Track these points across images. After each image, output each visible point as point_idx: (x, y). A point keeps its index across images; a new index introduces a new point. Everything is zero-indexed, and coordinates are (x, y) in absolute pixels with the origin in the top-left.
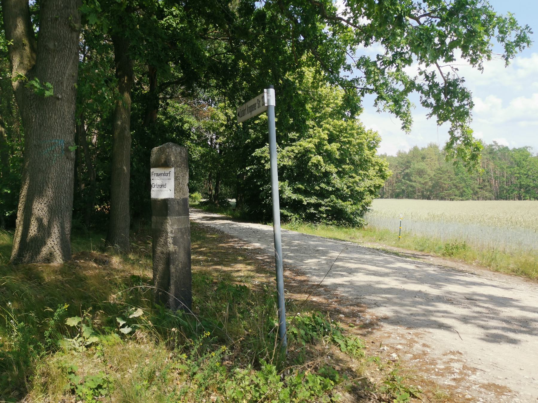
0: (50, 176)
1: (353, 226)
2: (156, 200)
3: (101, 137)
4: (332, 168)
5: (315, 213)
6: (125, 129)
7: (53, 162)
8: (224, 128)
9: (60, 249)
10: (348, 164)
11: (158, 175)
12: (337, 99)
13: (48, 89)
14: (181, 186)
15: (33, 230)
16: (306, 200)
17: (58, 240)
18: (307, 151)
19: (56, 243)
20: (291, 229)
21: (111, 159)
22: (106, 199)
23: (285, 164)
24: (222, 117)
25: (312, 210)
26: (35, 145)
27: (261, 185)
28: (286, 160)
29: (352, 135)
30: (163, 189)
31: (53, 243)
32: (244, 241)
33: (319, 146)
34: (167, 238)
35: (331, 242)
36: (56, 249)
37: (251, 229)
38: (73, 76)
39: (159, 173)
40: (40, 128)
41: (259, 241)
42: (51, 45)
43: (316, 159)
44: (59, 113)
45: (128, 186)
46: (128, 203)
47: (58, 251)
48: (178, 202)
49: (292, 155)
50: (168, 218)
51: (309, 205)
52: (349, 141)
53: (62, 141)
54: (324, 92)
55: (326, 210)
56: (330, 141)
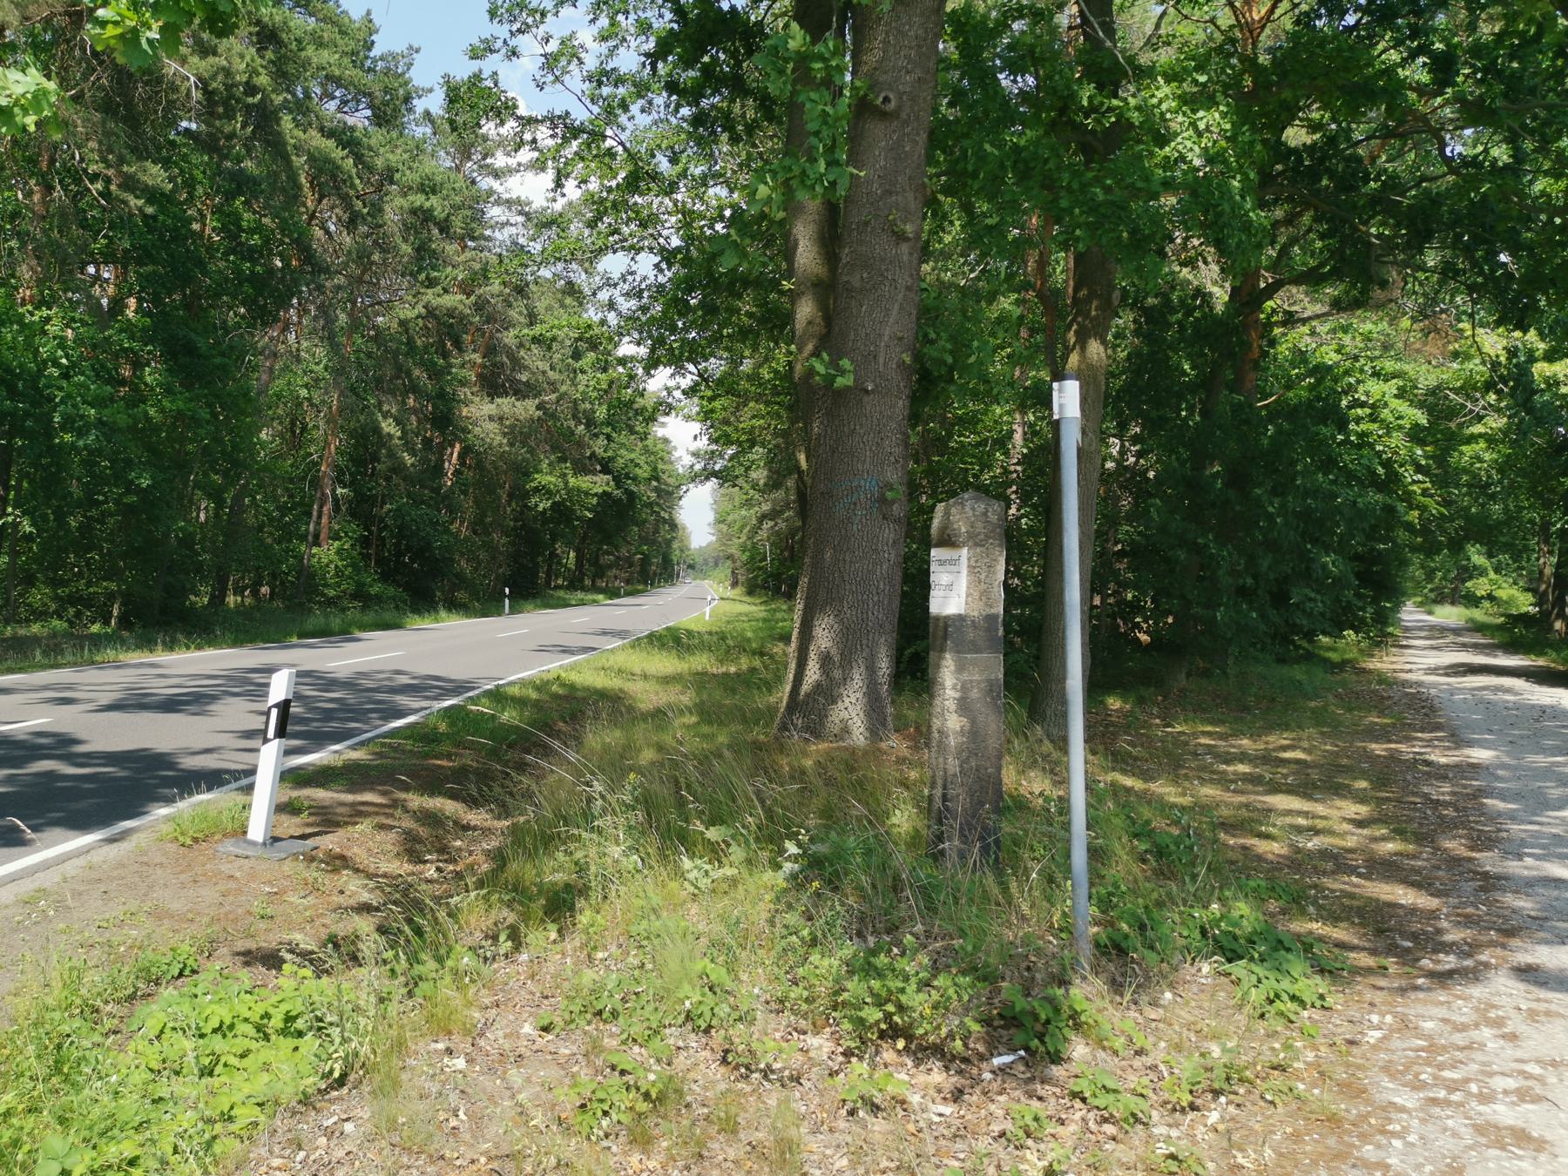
2: (937, 618)
11: (942, 563)
13: (843, 373)
15: (813, 674)
42: (856, 281)
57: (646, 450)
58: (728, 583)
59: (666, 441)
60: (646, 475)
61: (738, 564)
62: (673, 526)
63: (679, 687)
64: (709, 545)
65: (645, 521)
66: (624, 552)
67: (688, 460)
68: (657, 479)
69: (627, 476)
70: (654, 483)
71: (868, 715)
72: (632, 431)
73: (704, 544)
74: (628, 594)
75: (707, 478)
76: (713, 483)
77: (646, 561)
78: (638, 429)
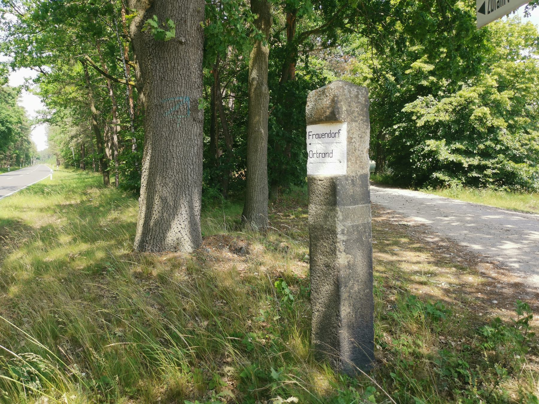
0: (174, 144)
1: (529, 192)
3: (238, 100)
4: (500, 122)
5: (479, 178)
6: (262, 84)
7: (178, 125)
8: (368, 81)
9: (188, 234)
10: (523, 117)
12: (512, 36)
14: (357, 153)
16: (467, 162)
17: (186, 223)
18: (470, 102)
19: (183, 226)
20: (451, 196)
21: (247, 124)
22: (243, 164)
23: (441, 119)
24: (366, 70)
25: (475, 174)
26: (156, 105)
27: (412, 146)
28: (442, 114)
29: (531, 80)
30: (328, 159)
31: (179, 227)
32: (399, 214)
33: (484, 97)
34: (335, 243)
35: (517, 215)
36: (184, 234)
37: (402, 197)
38: (199, 12)
39: (320, 132)
40: (161, 83)
41: (418, 214)
43: (479, 111)
44: (183, 62)
45: (265, 152)
46: (266, 172)
47: (185, 237)
48: (352, 180)
49: (450, 108)
50: (338, 209)
51: (471, 168)
52: (526, 87)
53: (187, 99)
54: (494, 28)
55: (494, 174)
56: (501, 89)
57: (15, 111)
58: (55, 165)
59: (23, 108)
60: (16, 121)
61: (60, 157)
62: (29, 143)
63: (50, 213)
64: (45, 150)
65: (16, 141)
66: (8, 153)
67: (35, 115)
68: (21, 123)
69: (7, 121)
70: (20, 125)
71: (191, 233)
72: (7, 102)
73: (43, 150)
74: (11, 170)
75: (44, 122)
76: (46, 124)
77: (18, 157)
78: (10, 102)
